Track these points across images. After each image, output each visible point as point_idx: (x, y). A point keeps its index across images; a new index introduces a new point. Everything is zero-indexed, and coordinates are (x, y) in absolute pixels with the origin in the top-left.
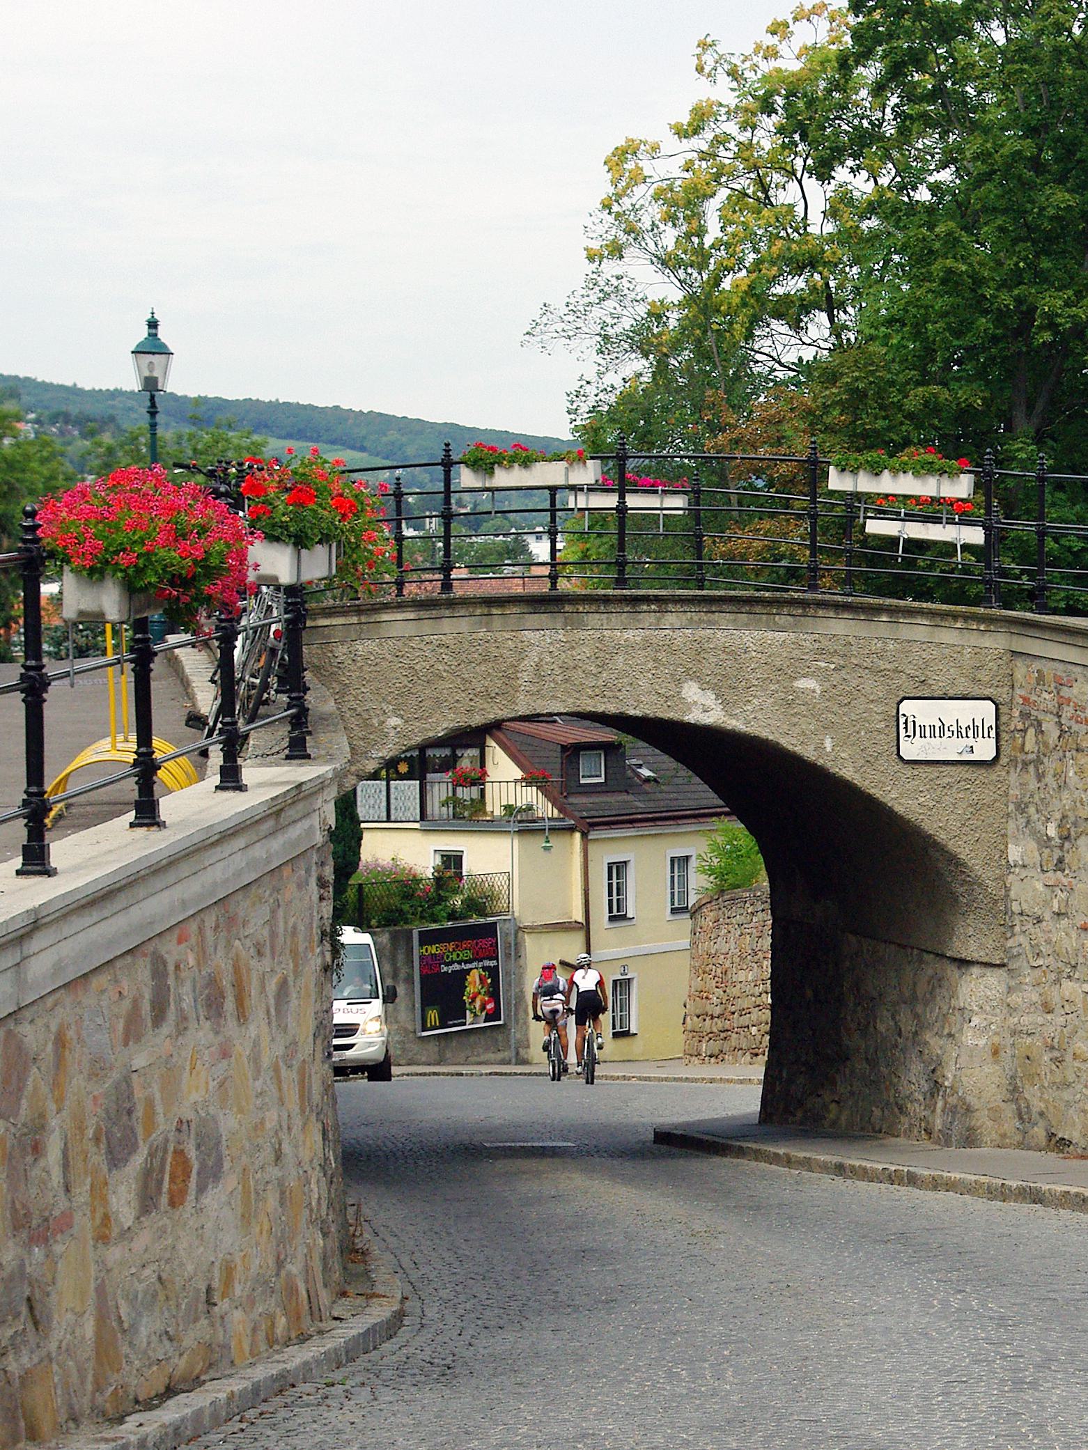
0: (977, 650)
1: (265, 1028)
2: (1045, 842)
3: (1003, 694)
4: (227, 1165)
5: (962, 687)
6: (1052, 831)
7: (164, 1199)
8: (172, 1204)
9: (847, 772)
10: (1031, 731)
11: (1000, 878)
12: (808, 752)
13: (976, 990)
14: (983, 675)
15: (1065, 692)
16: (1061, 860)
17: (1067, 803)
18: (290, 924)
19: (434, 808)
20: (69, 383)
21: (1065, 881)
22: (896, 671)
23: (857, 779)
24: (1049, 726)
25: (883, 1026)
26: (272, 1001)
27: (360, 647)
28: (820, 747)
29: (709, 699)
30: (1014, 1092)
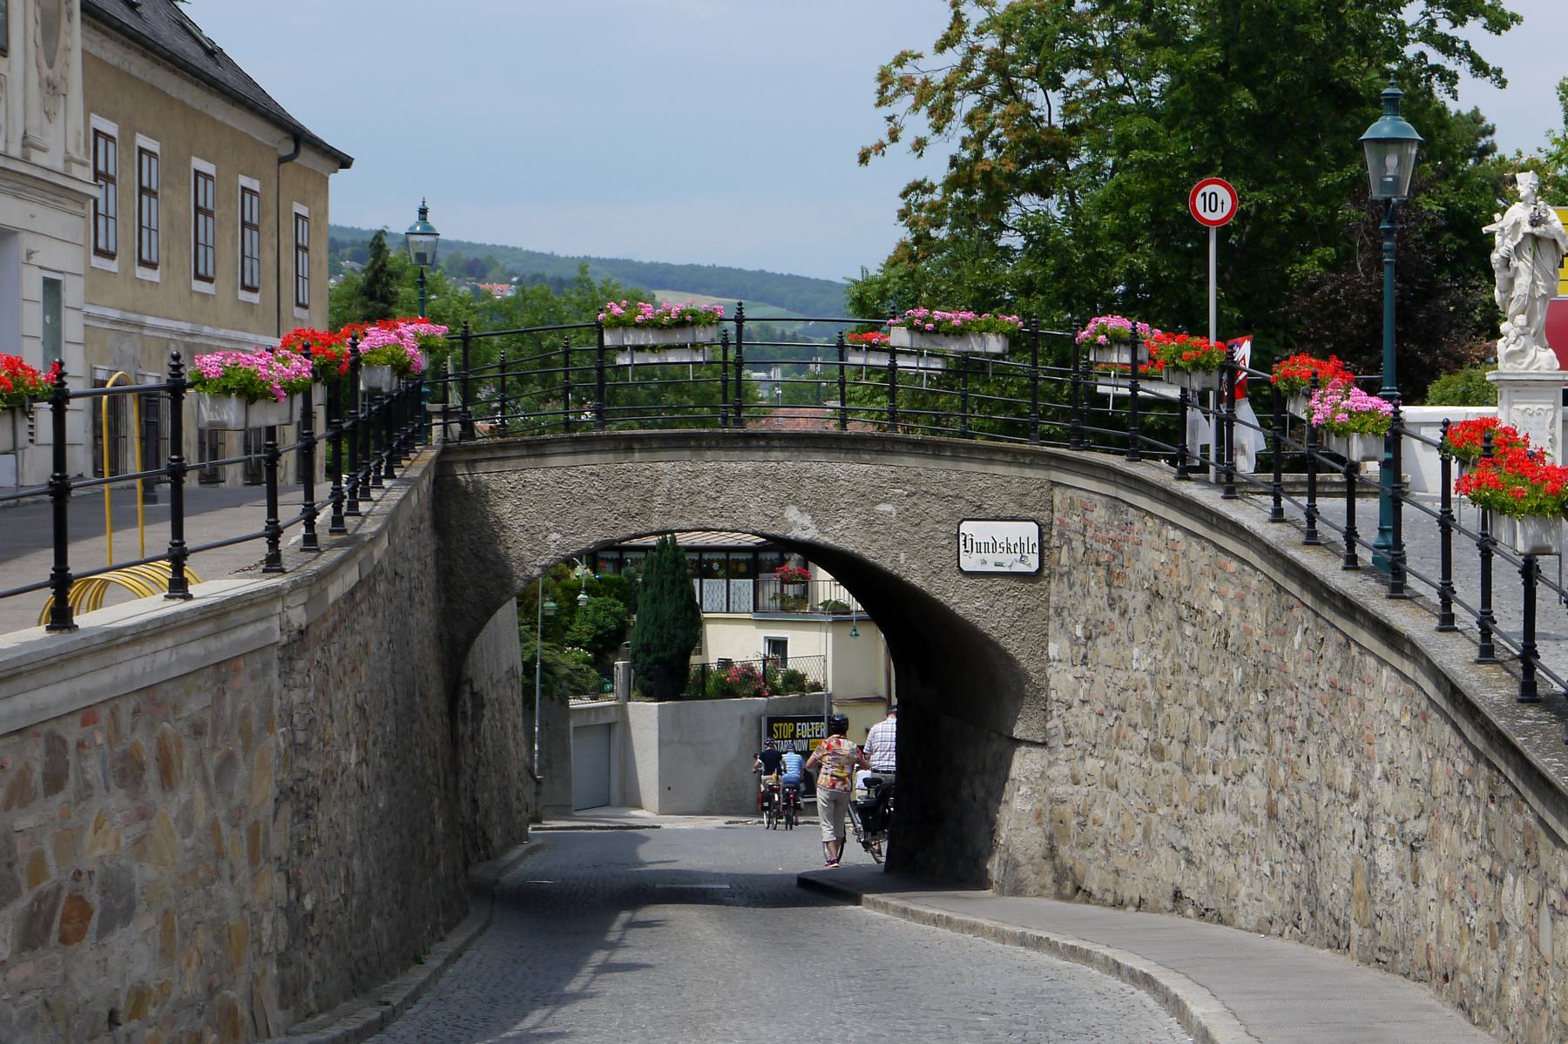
0: (1024, 481)
1: (199, 794)
2: (1074, 641)
3: (1044, 516)
4: (140, 909)
5: (1012, 509)
6: (1079, 632)
7: (54, 938)
8: (64, 940)
9: (916, 581)
10: (1065, 548)
11: (1042, 670)
12: (887, 564)
13: (1023, 764)
14: (1028, 501)
15: (1089, 515)
16: (1085, 657)
17: (1090, 608)
18: (242, 706)
19: (765, 601)
20: (547, 251)
21: (1088, 674)
22: (957, 497)
23: (925, 587)
24: (1077, 544)
25: (965, 793)
26: (211, 772)
27: (528, 476)
28: (895, 559)
29: (806, 520)
30: (1051, 853)
